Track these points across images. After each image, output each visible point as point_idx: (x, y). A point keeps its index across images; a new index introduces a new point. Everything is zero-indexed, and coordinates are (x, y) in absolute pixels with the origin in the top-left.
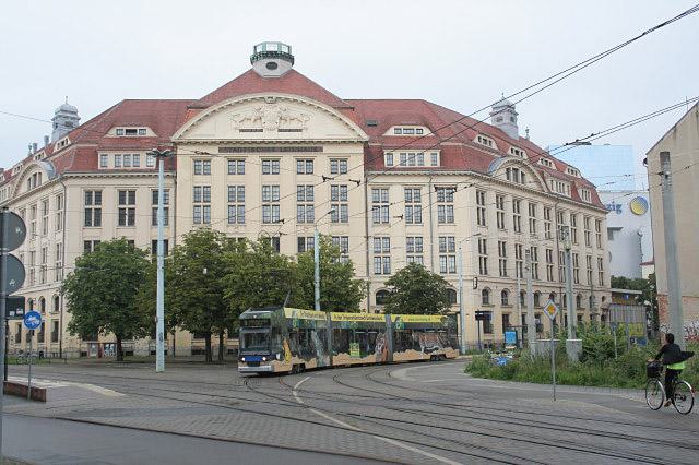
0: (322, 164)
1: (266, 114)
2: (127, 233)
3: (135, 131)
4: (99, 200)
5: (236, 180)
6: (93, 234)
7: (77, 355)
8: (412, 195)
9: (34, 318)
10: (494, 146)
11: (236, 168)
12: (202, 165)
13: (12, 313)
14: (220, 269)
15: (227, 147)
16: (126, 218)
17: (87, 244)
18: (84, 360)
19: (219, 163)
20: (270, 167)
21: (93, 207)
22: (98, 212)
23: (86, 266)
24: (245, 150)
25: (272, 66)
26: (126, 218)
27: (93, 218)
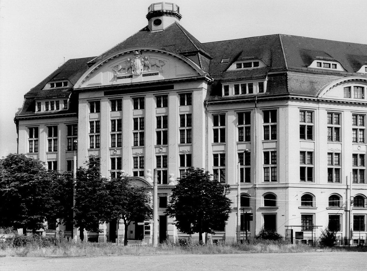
12: (95, 106)
20: (139, 104)
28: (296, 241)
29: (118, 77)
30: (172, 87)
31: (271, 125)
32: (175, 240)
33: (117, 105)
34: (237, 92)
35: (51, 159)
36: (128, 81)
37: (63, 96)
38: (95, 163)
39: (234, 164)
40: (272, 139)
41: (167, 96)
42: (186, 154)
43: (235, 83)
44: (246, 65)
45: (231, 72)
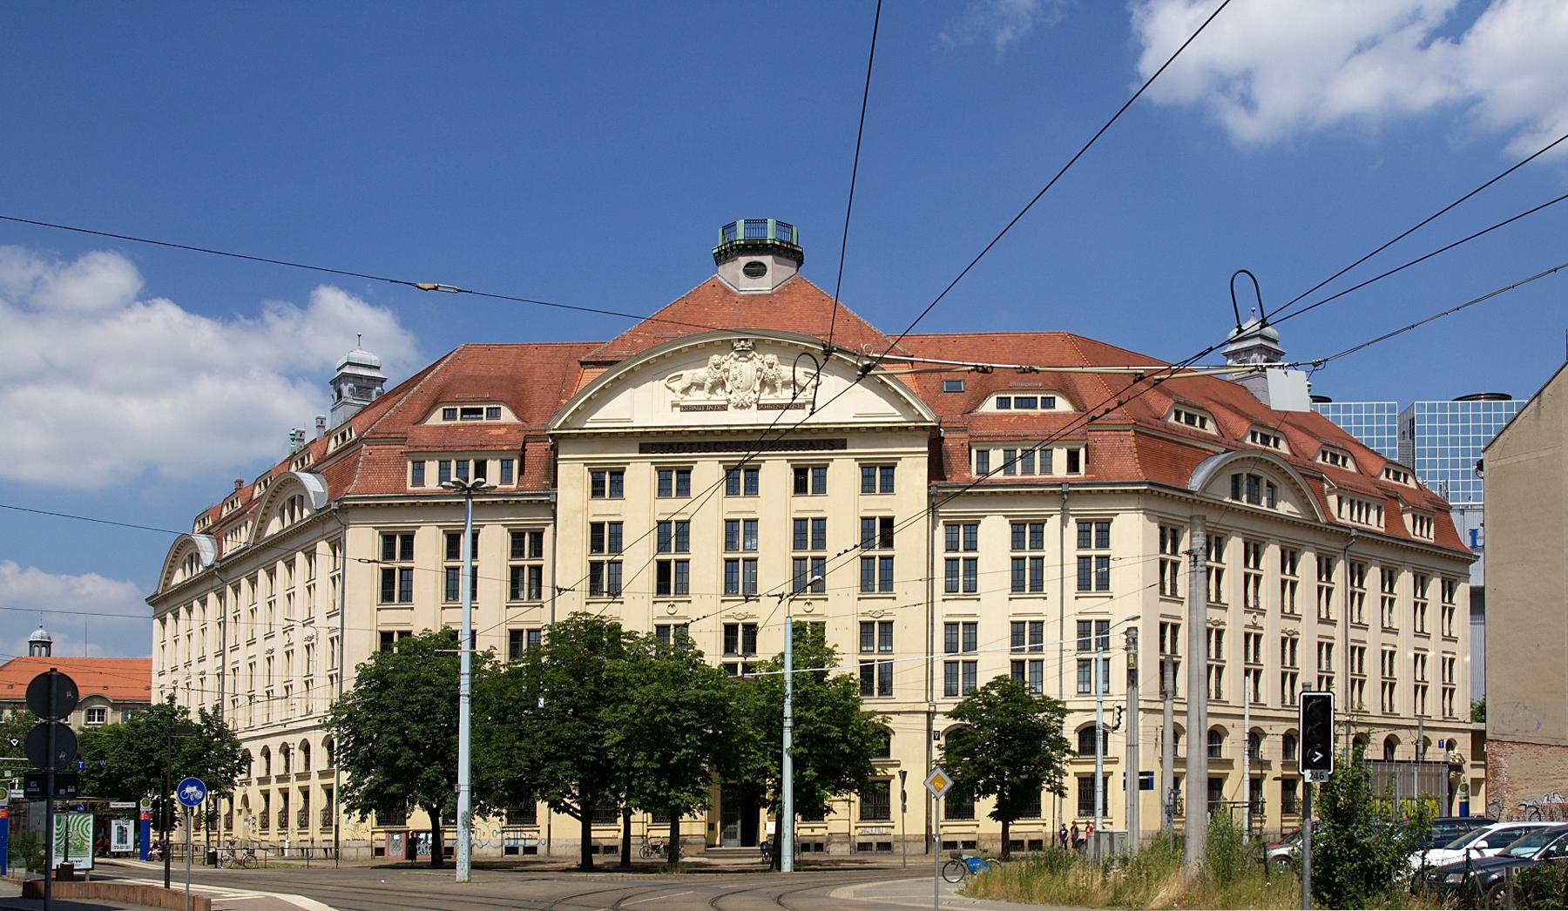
0: (843, 471)
1: (734, 372)
2: (456, 618)
3: (480, 411)
4: (683, 544)
5: (741, 507)
6: (395, 619)
7: (368, 852)
8: (1027, 533)
9: (194, 789)
10: (1210, 428)
11: (675, 482)
12: (606, 482)
13: (62, 791)
14: (606, 692)
15: (653, 442)
16: (603, 580)
17: (386, 637)
18: (379, 861)
19: (641, 474)
20: (741, 480)
21: (809, 553)
22: (407, 573)
23: (376, 680)
24: (691, 447)
25: (755, 271)
26: (603, 580)
27: (394, 587)
28: (1023, 841)
29: (684, 407)
30: (842, 444)
31: (399, 568)
32: (65, 888)
33: (675, 482)
34: (1073, 465)
35: (959, 615)
36: (792, 418)
37: (498, 448)
38: (808, 638)
39: (1304, 639)
40: (880, 590)
41: (688, 471)
42: (879, 619)
43: (1007, 445)
44: (1021, 403)
45: (984, 415)
